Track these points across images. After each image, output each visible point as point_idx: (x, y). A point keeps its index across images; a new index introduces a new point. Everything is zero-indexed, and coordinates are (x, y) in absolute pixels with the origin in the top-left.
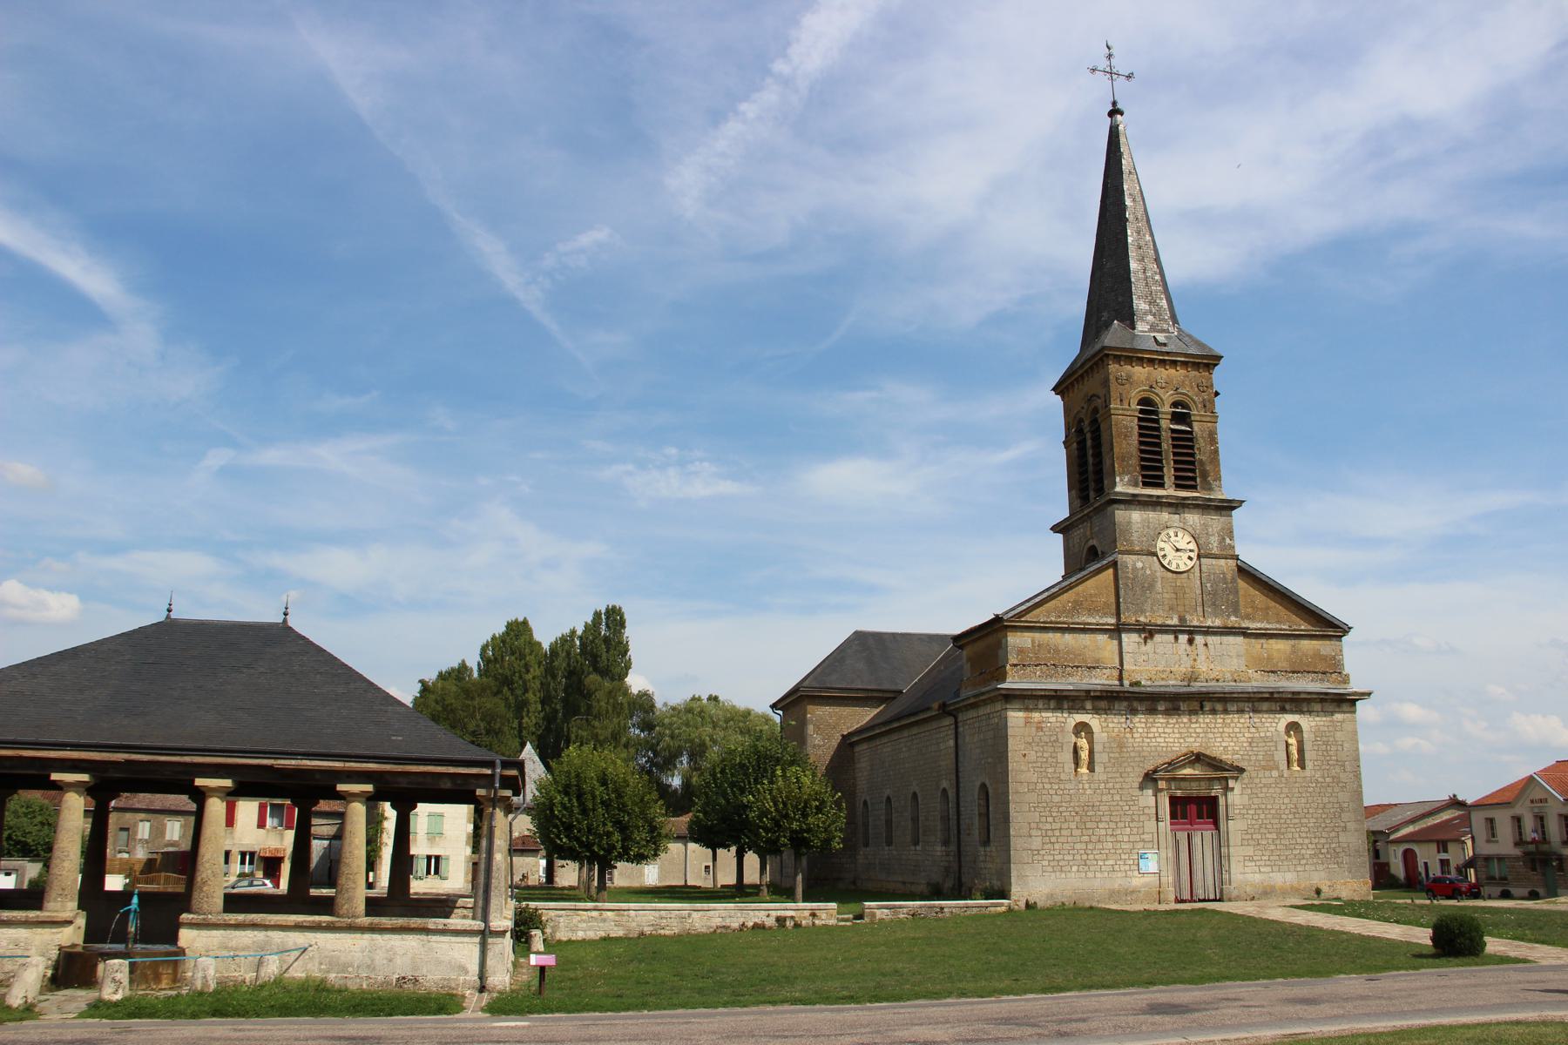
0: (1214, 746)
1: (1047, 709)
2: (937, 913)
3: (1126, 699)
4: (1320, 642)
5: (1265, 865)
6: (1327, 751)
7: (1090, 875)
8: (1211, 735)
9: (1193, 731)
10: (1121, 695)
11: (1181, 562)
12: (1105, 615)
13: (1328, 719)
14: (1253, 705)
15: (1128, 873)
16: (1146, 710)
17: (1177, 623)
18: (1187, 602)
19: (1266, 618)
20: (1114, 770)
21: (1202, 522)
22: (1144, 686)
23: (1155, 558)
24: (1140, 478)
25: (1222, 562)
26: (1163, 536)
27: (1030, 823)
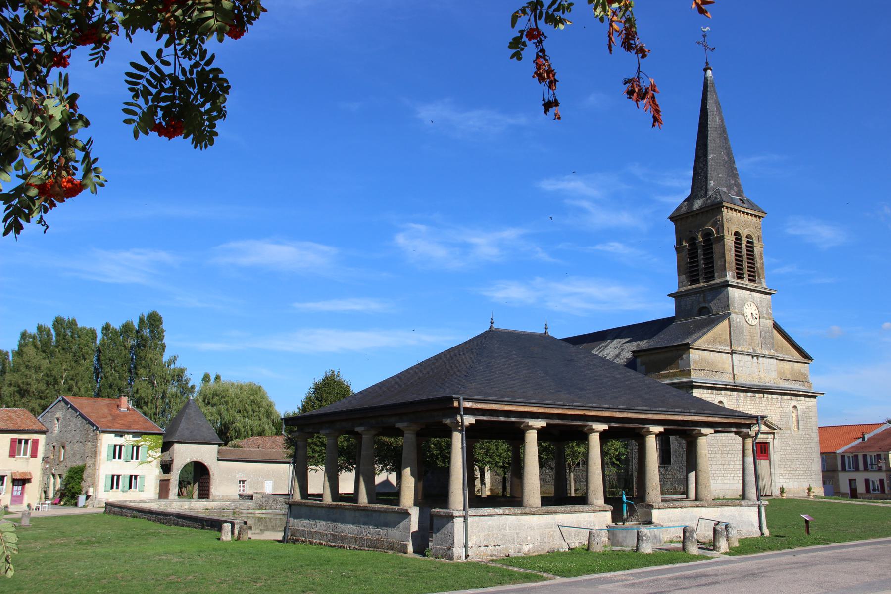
26: (746, 306)
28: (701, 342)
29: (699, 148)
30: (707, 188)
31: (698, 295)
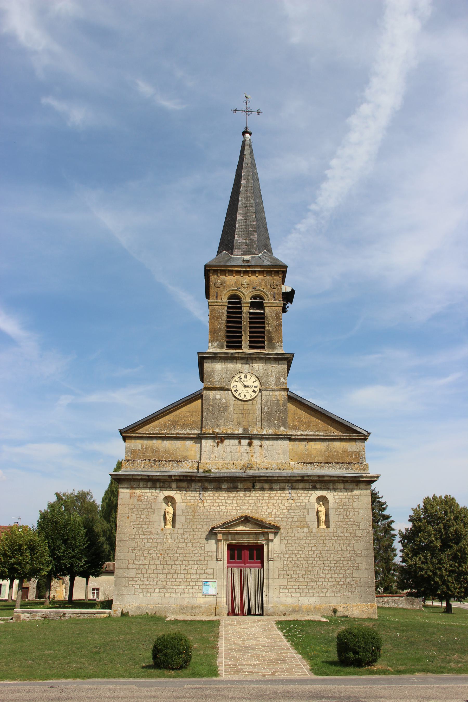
0: (262, 512)
1: (146, 488)
2: (61, 617)
3: (199, 481)
4: (348, 443)
5: (296, 592)
6: (346, 515)
7: (167, 595)
8: (260, 505)
9: (247, 502)
10: (193, 478)
11: (249, 394)
12: (193, 428)
13: (349, 494)
14: (292, 485)
15: (195, 594)
16: (214, 488)
17: (242, 433)
18: (250, 419)
19: (308, 428)
20: (189, 527)
21: (265, 369)
22: (213, 473)
23: (230, 392)
24: (225, 343)
25: (277, 393)
26: (236, 378)
27: (128, 560)
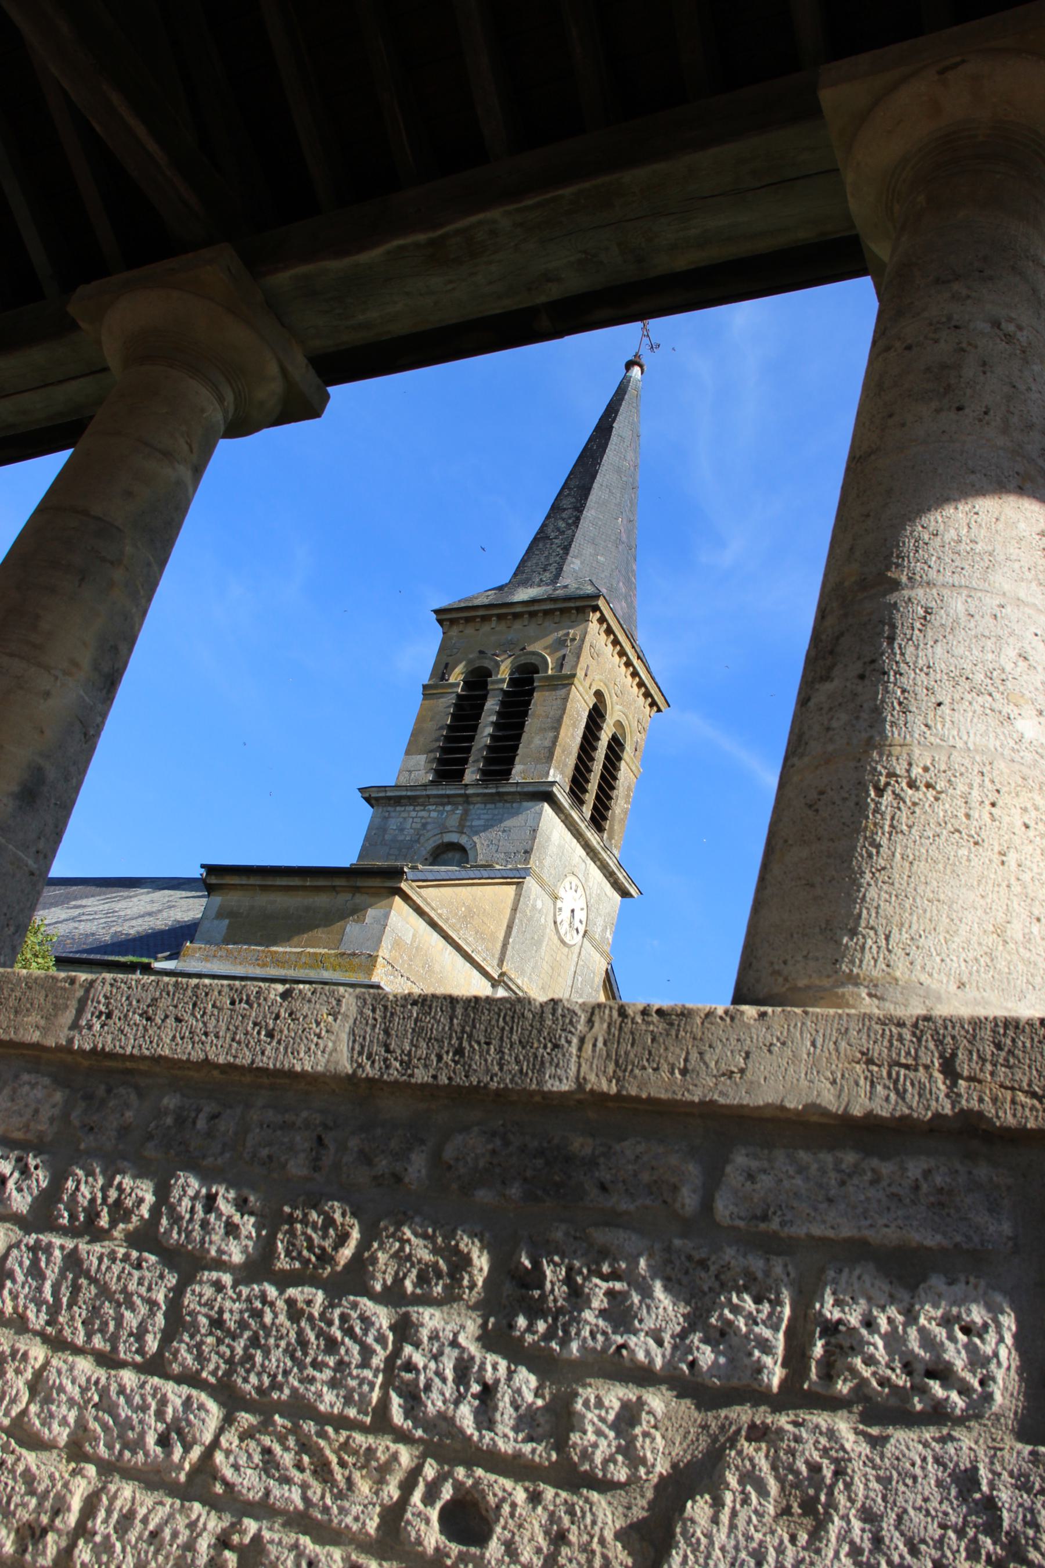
28: (433, 897)
29: (566, 492)
30: (561, 569)
31: (448, 808)
